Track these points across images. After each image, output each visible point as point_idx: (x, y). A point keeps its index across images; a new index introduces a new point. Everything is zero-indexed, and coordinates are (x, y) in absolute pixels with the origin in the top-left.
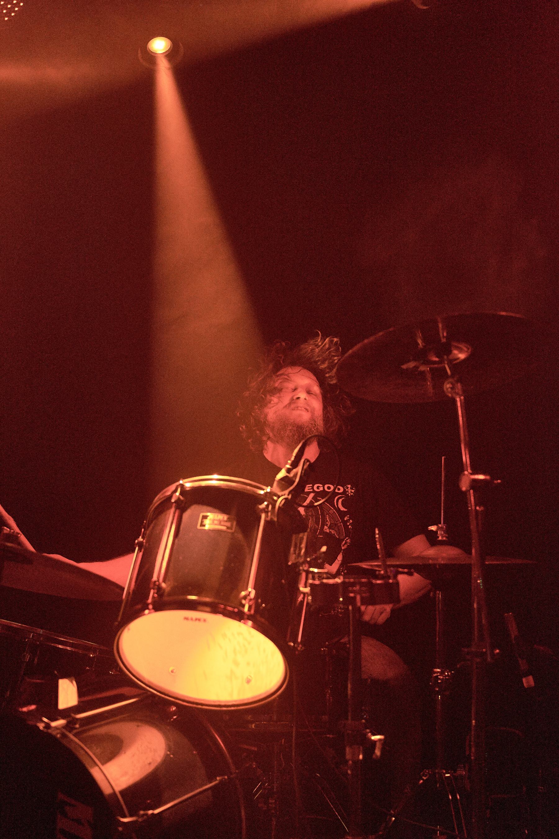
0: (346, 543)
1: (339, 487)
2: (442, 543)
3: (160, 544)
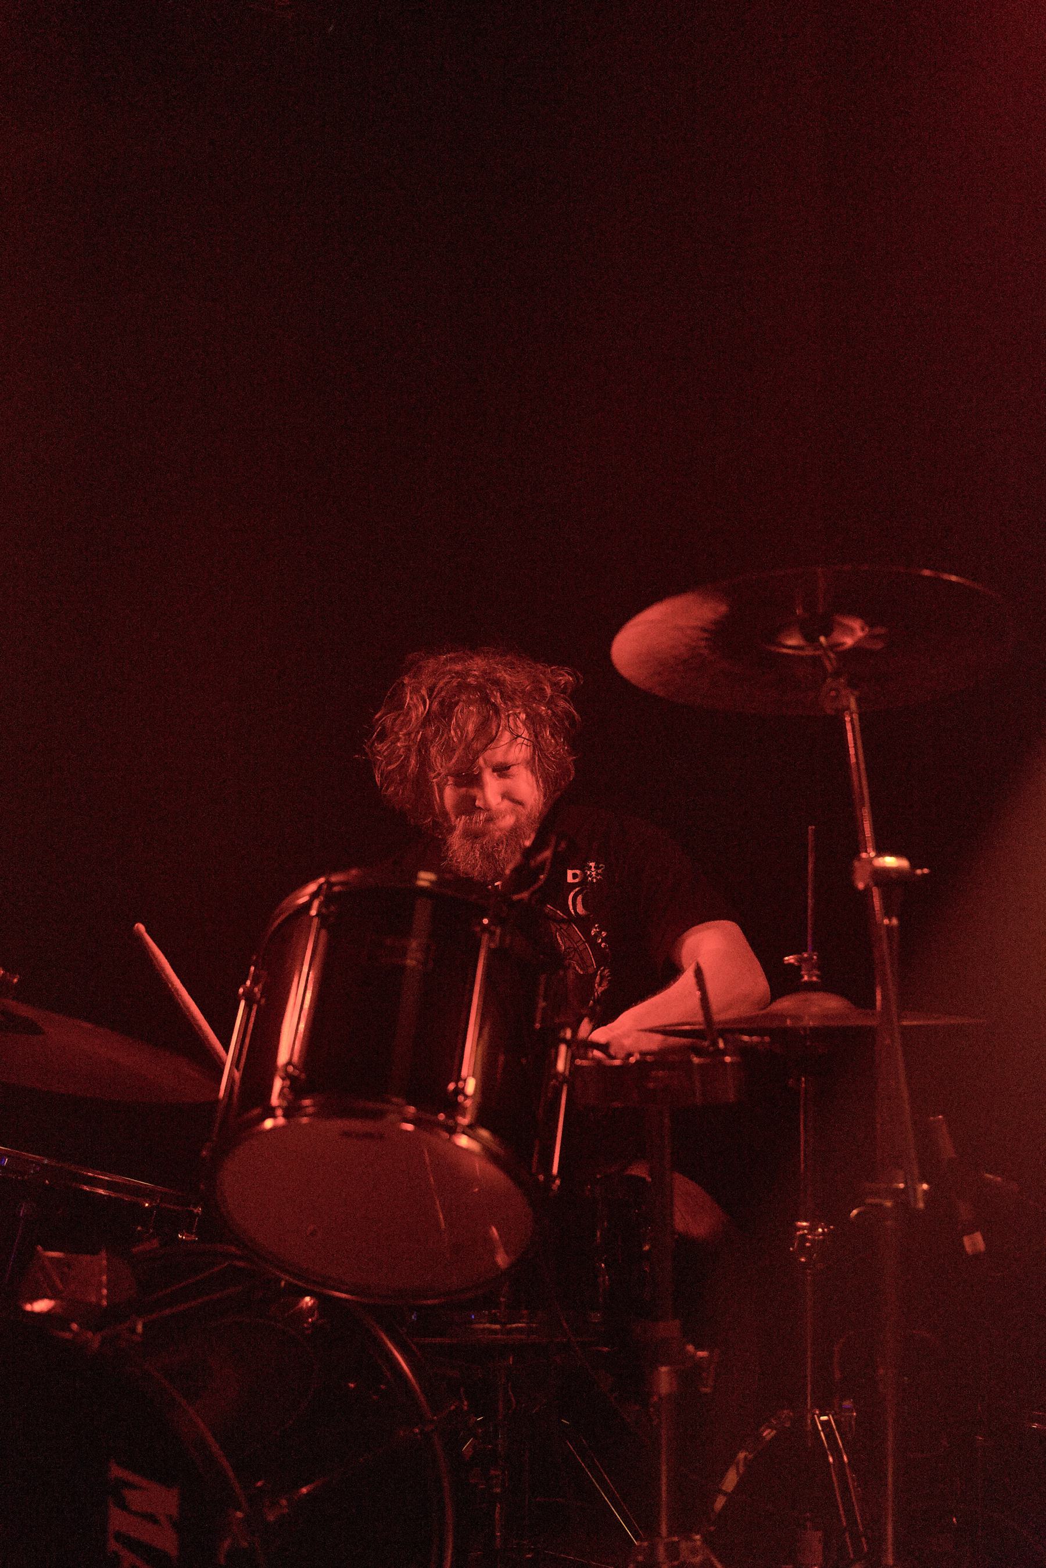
0: (602, 978)
1: (577, 880)
2: (811, 987)
3: (281, 1023)
